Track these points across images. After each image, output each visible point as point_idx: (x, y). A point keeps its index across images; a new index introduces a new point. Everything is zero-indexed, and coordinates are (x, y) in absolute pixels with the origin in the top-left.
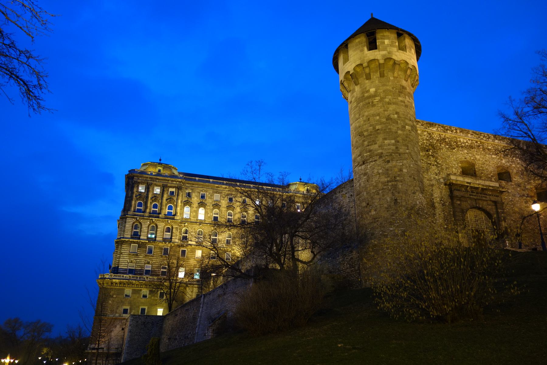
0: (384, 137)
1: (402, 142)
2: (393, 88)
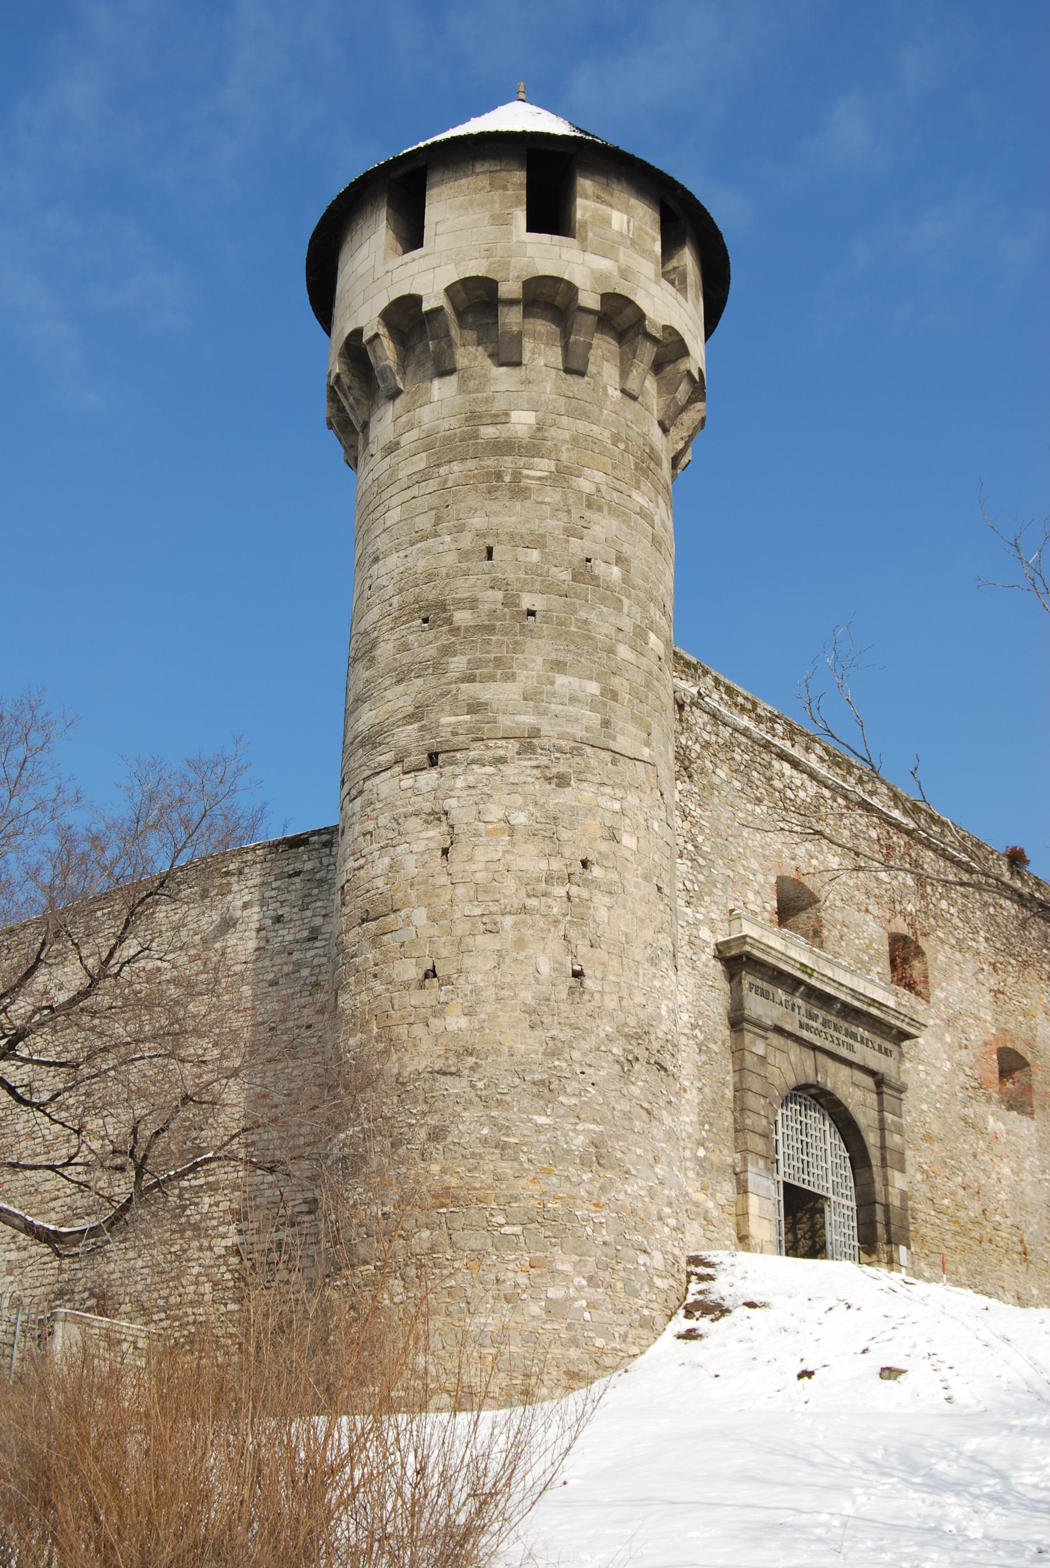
0: (553, 656)
1: (630, 701)
2: (616, 439)
